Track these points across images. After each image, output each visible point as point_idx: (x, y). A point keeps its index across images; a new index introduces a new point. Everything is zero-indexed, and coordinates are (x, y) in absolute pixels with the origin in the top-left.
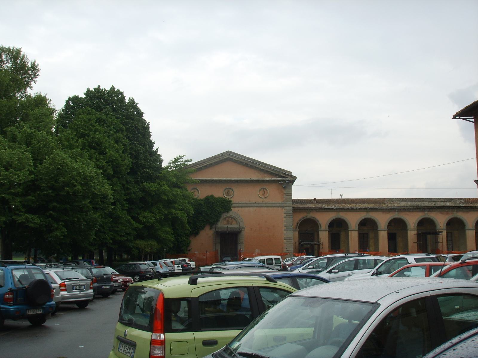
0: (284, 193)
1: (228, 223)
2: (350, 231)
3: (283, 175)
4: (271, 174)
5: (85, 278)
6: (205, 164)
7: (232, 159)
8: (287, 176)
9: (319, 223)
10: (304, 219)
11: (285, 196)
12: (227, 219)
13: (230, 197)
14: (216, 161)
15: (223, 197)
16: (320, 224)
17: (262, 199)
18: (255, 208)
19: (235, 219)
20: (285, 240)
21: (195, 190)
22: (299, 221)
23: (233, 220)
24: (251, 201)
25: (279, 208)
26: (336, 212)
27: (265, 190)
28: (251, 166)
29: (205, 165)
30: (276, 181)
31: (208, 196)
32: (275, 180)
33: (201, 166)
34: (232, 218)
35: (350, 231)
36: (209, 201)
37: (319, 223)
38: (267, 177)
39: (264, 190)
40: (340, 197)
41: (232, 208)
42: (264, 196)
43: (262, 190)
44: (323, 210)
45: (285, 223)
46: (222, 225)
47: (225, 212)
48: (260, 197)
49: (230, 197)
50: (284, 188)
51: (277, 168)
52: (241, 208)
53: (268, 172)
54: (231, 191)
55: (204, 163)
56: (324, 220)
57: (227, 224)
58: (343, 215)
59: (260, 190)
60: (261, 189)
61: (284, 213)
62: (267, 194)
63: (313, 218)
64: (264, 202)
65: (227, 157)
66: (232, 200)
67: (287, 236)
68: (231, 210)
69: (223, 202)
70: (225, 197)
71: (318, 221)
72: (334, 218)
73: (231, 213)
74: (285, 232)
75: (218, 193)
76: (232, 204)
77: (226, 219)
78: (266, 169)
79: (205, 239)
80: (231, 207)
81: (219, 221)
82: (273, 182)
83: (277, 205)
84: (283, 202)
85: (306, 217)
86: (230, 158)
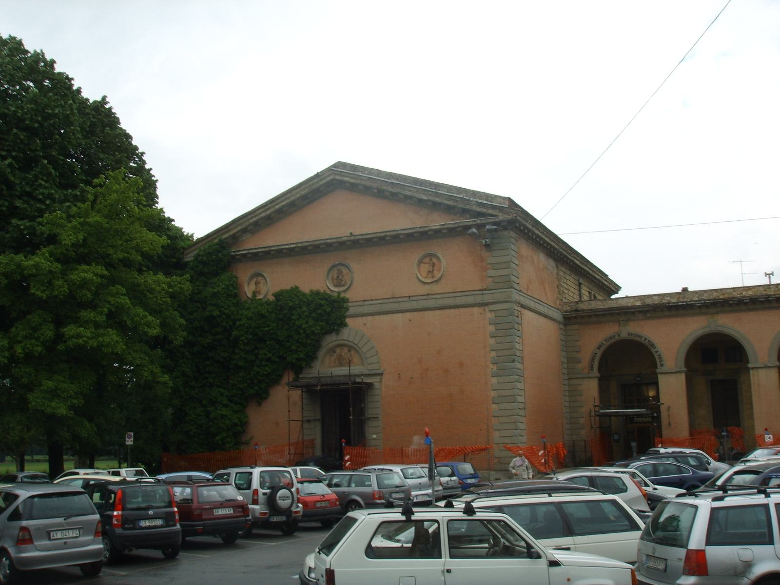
0: (489, 262)
1: (341, 362)
2: (753, 368)
3: (478, 209)
4: (449, 210)
5: (331, 493)
6: (277, 204)
7: (345, 182)
8: (490, 212)
9: (657, 352)
10: (613, 340)
11: (491, 273)
12: (338, 350)
13: (342, 289)
14: (303, 193)
15: (325, 291)
16: (659, 355)
17: (427, 287)
18: (408, 315)
19: (357, 351)
20: (494, 406)
21: (260, 278)
22: (598, 348)
23: (352, 352)
24: (396, 296)
25: (476, 310)
26: (706, 314)
27: (434, 260)
28: (392, 194)
29: (277, 207)
30: (461, 229)
31: (282, 290)
32: (456, 225)
33: (268, 212)
34: (350, 348)
35: (753, 368)
36: (288, 304)
37: (657, 352)
38: (437, 221)
39: (431, 260)
40: (765, 281)
41: (347, 320)
42: (433, 277)
43: (427, 260)
44: (667, 313)
45: (493, 354)
46: (326, 368)
47: (329, 332)
48: (421, 281)
49: (342, 289)
50: (487, 246)
51: (363, 169)
52: (370, 318)
53: (440, 204)
54: (345, 271)
55: (274, 204)
56: (671, 341)
57: (338, 366)
58: (729, 324)
59: (420, 262)
60: (425, 256)
61: (490, 324)
62: (439, 270)
63: (638, 339)
64: (433, 294)
65: (329, 179)
66: (347, 295)
67: (502, 393)
68: (346, 325)
69: (321, 305)
70: (331, 290)
71: (653, 345)
72: (700, 333)
73: (346, 335)
74: (494, 380)
75: (311, 279)
76: (347, 309)
77: (334, 352)
78: (430, 198)
79: (282, 410)
80: (345, 317)
81: (317, 358)
82: (452, 232)
83: (470, 300)
84: (485, 290)
85: (617, 337)
86: (338, 180)
